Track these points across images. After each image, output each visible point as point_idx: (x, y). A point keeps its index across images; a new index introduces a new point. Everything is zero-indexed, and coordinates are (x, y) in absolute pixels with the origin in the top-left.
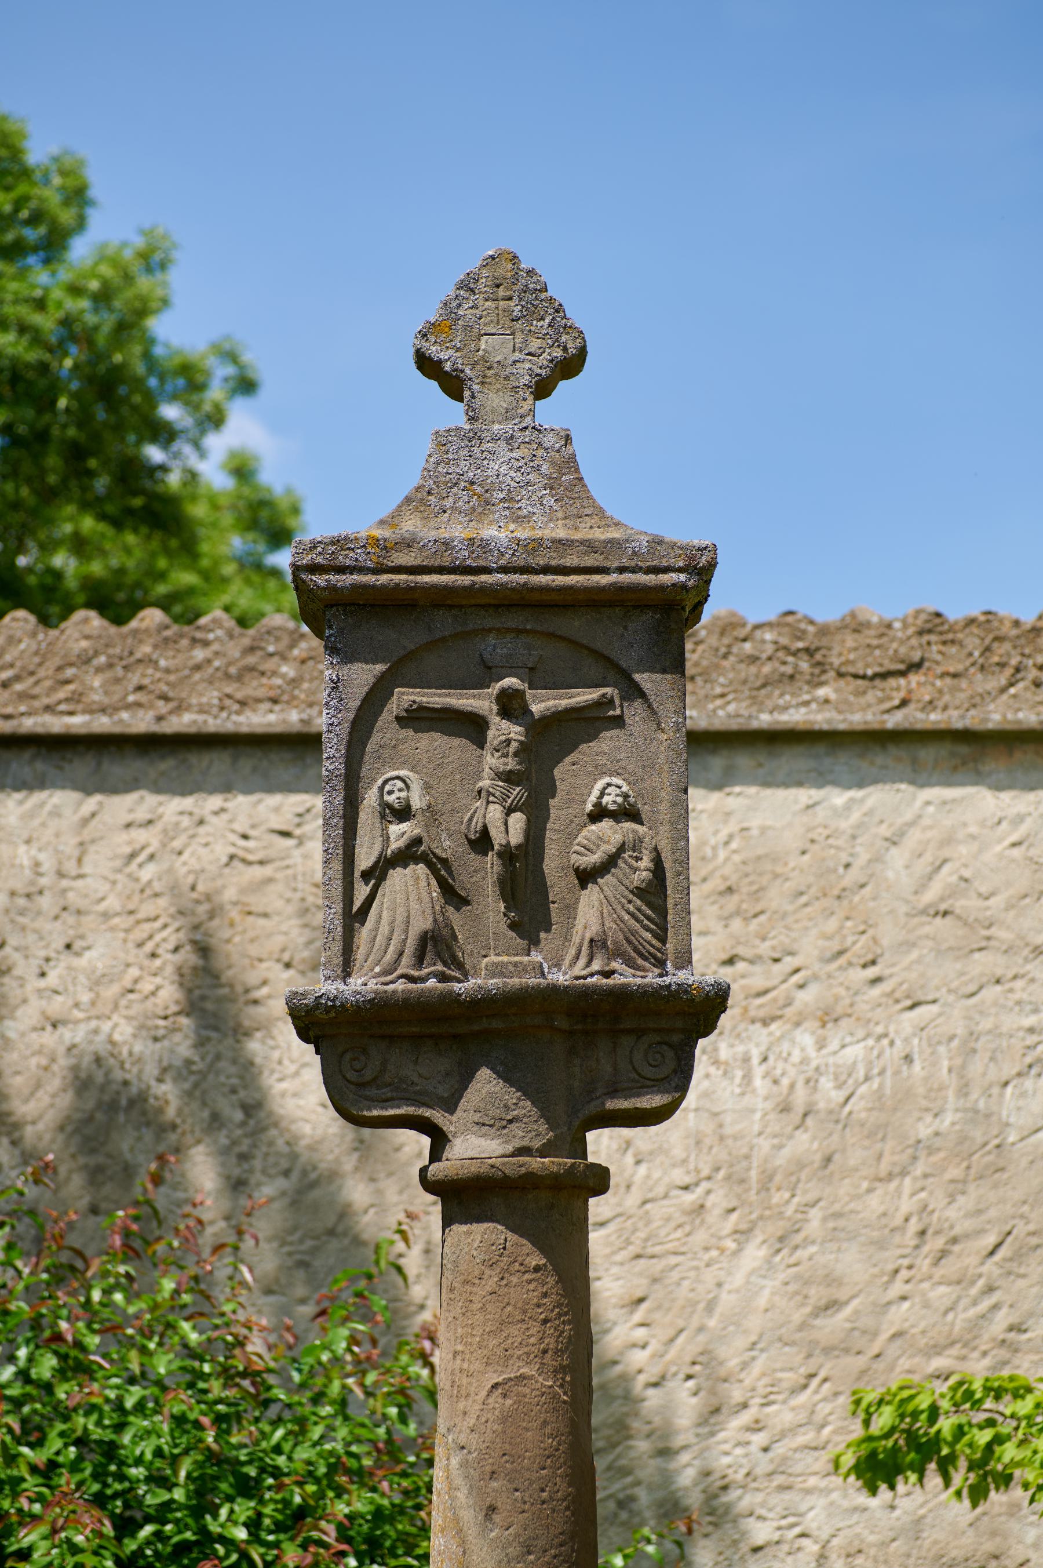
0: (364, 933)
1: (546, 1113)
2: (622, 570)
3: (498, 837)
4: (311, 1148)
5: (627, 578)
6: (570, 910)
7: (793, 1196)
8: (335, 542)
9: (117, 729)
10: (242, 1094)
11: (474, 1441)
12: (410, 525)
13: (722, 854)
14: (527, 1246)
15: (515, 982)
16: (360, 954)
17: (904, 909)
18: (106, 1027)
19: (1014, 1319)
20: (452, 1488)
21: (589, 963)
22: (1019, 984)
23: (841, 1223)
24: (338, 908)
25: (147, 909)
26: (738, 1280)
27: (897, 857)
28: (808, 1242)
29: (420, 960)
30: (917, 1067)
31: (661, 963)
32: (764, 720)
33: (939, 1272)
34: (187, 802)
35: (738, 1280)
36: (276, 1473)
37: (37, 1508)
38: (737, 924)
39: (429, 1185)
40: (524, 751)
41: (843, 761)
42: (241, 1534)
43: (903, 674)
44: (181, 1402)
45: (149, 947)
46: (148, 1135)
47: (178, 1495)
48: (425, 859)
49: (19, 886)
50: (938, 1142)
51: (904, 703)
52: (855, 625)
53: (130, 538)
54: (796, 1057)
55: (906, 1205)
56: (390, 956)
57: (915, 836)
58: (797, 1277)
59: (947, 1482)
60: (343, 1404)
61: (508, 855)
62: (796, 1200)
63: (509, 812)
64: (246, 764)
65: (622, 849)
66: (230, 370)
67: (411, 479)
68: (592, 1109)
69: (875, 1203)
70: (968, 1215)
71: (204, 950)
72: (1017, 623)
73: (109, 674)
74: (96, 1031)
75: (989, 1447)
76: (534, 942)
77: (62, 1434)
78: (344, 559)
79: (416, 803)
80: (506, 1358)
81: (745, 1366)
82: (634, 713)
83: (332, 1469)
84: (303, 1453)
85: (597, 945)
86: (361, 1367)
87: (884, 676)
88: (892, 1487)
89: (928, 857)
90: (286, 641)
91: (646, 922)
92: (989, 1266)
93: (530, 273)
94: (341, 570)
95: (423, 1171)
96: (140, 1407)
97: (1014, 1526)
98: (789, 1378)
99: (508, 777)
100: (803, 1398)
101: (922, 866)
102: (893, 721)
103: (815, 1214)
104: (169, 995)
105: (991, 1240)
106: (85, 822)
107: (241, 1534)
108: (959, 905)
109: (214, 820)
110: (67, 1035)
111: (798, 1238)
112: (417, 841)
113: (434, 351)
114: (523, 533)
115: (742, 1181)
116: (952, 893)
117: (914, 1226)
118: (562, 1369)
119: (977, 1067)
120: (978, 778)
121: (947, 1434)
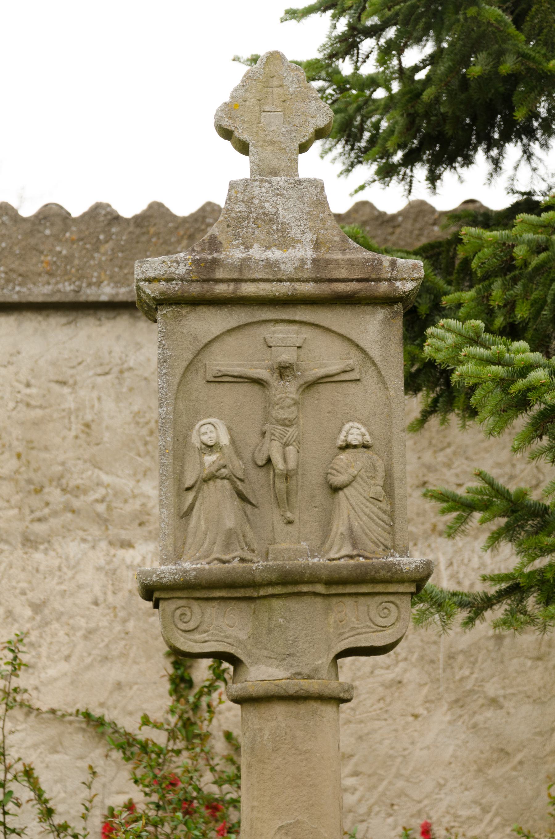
7: (472, 673)
10: (30, 595)
21: (339, 550)
62: (475, 676)
91: (378, 521)
115: (432, 662)
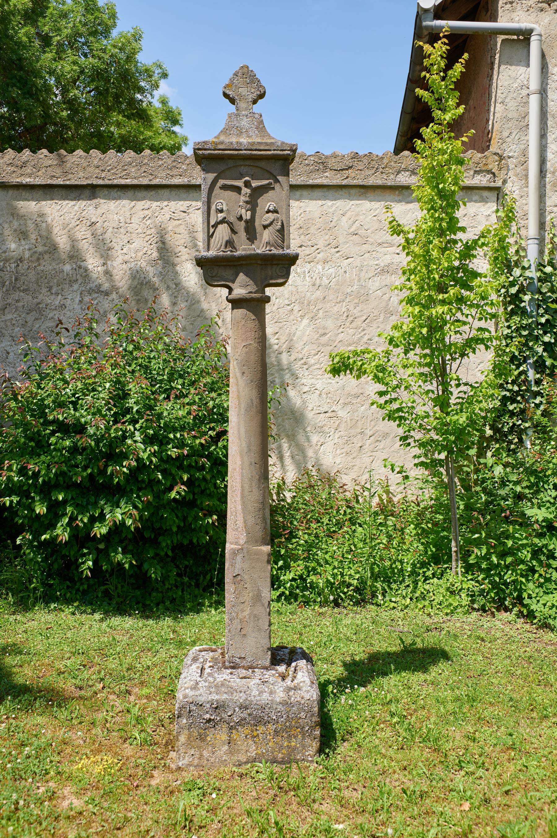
0: (212, 240)
1: (256, 283)
2: (274, 150)
3: (244, 217)
4: (193, 295)
5: (276, 152)
6: (262, 235)
8: (204, 142)
9: (139, 183)
11: (239, 358)
12: (222, 138)
13: (299, 218)
14: (251, 314)
15: (248, 252)
16: (211, 246)
17: (346, 233)
18: (139, 263)
19: (369, 337)
20: (234, 368)
22: (374, 253)
23: (327, 314)
24: (206, 234)
25: (149, 232)
26: (301, 328)
27: (344, 219)
28: (319, 318)
29: (226, 247)
30: (348, 274)
31: (283, 248)
32: (311, 182)
33: (351, 326)
34: (158, 203)
35: (301, 328)
36: (188, 373)
37: (131, 380)
38: (302, 237)
39: (229, 300)
40: (250, 196)
41: (331, 193)
42: (180, 387)
43: (347, 169)
44: (165, 356)
45: (150, 242)
46: (151, 291)
47: (165, 377)
48: (227, 222)
49: (116, 226)
50: (352, 293)
51: (347, 177)
52: (335, 156)
53: (133, 122)
54: (317, 272)
55: (344, 309)
56: (219, 246)
57: (349, 213)
58: (316, 327)
59: (351, 373)
60: (203, 357)
61: (247, 222)
63: (247, 211)
64: (174, 193)
65: (274, 220)
66: (160, 71)
67: (222, 126)
68: (266, 283)
69: (336, 309)
70: (359, 312)
71: (164, 243)
72: (377, 156)
73: (136, 168)
74: (137, 264)
75: (361, 366)
76: (253, 243)
77: (136, 364)
78: (206, 147)
79: (225, 209)
80: (247, 339)
81: (302, 349)
82: (277, 186)
83: (201, 372)
84: (194, 368)
85: (268, 243)
86: (208, 348)
87: (342, 170)
88: (339, 376)
89: (352, 219)
90: (183, 159)
92: (364, 325)
93: (252, 71)
94: (205, 150)
95: (227, 297)
96: (154, 357)
97: (367, 386)
98: (313, 352)
99: (247, 202)
100: (317, 357)
101: (350, 222)
102: (344, 182)
103: (321, 311)
104: (155, 255)
105: (364, 318)
106: (132, 208)
107: (180, 387)
108: (360, 232)
109: (165, 208)
110: (129, 265)
111: (316, 318)
112: (225, 218)
113: (228, 92)
114: (250, 141)
116: (358, 229)
117: (345, 314)
118: (260, 342)
119: (363, 274)
120: (366, 198)
121: (351, 363)
